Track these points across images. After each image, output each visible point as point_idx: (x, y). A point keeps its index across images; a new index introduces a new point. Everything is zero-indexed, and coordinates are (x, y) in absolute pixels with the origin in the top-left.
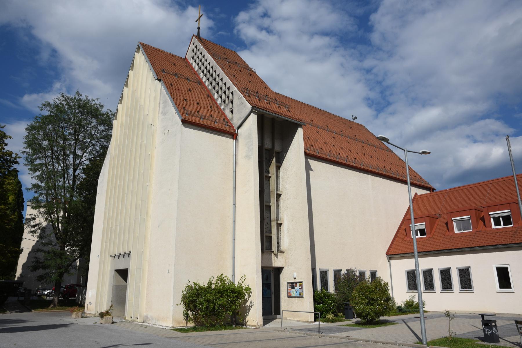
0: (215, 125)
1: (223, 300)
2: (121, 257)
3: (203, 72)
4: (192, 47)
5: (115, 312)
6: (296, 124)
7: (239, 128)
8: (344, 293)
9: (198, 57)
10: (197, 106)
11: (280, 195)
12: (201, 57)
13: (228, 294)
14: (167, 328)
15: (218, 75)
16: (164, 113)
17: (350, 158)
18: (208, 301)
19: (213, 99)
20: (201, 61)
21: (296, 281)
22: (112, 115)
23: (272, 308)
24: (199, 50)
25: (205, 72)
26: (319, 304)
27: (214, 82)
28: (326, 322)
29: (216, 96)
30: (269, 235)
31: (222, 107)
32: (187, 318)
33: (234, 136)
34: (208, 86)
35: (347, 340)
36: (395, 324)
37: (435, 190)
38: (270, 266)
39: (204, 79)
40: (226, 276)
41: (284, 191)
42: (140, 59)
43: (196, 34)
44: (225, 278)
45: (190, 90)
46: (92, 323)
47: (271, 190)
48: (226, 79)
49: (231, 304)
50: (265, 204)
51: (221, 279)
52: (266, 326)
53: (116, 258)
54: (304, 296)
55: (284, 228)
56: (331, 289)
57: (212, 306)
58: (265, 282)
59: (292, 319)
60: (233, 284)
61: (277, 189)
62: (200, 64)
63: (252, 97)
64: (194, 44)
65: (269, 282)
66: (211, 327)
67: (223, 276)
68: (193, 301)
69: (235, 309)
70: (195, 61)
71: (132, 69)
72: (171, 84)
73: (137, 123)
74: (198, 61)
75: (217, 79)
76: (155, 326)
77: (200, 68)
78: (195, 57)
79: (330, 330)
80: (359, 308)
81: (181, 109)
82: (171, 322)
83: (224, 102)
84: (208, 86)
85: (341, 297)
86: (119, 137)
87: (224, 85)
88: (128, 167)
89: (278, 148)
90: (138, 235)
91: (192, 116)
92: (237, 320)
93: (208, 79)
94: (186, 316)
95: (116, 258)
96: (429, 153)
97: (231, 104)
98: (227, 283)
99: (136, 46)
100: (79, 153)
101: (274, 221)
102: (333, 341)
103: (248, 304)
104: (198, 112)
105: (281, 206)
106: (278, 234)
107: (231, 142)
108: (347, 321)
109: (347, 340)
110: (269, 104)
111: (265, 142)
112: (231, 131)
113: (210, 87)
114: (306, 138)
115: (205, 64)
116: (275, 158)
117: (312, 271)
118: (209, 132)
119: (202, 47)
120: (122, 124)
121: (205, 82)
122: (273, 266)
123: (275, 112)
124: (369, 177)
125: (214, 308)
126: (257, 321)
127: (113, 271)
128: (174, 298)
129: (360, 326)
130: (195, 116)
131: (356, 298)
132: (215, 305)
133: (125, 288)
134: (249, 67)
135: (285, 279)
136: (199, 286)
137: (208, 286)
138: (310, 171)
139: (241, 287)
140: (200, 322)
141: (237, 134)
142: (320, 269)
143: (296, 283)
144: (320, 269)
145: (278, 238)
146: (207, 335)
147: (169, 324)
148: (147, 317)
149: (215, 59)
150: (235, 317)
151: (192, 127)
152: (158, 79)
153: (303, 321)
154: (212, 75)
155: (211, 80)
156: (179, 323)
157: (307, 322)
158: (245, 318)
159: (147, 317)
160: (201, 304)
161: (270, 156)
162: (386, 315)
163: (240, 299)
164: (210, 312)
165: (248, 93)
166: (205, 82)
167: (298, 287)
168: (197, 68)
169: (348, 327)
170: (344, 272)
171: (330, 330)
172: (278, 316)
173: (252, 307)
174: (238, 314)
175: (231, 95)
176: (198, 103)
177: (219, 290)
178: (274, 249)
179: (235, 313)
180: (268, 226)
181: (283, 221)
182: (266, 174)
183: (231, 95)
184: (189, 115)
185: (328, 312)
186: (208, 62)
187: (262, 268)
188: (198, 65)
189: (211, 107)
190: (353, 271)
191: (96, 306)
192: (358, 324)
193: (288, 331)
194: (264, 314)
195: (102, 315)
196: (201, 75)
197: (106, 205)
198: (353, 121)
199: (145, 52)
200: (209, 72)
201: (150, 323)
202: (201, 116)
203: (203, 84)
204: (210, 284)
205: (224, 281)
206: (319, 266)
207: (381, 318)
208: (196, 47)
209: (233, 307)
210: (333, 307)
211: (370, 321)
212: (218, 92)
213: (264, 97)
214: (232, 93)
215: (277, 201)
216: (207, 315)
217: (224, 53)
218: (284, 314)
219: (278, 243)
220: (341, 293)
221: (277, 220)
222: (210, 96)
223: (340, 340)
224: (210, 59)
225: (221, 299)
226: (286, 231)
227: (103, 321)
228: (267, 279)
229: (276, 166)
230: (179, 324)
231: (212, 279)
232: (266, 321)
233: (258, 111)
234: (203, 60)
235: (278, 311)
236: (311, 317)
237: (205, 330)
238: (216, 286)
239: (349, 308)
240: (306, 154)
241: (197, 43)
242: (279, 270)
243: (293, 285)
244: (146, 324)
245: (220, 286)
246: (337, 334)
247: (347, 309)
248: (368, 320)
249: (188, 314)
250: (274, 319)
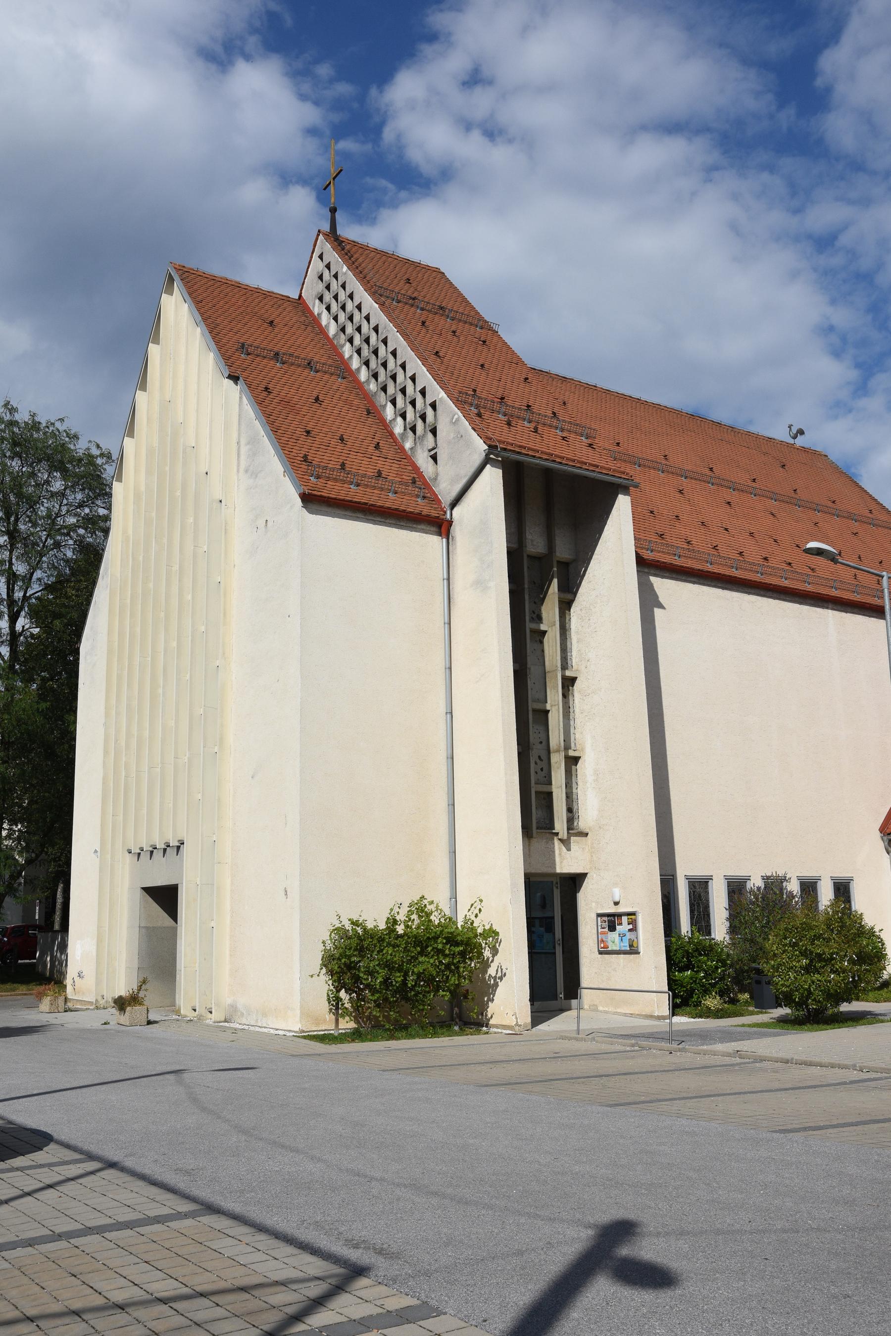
0: (391, 500)
1: (426, 964)
2: (158, 855)
3: (351, 340)
4: (317, 266)
5: (150, 997)
6: (612, 484)
7: (454, 504)
8: (752, 941)
9: (336, 297)
10: (340, 446)
11: (573, 680)
12: (342, 296)
13: (440, 946)
14: (288, 1034)
15: (394, 353)
16: (253, 473)
17: (773, 562)
18: (388, 965)
19: (382, 420)
20: (343, 308)
21: (621, 909)
22: (102, 455)
23: (555, 980)
24: (336, 276)
25: (357, 340)
26: (681, 970)
27: (381, 371)
28: (701, 1017)
29: (389, 412)
30: (544, 788)
31: (408, 445)
32: (337, 1008)
33: (441, 526)
34: (368, 381)
35: (738, 1060)
36: (882, 1021)
38: (550, 871)
39: (355, 363)
40: (432, 903)
41: (582, 668)
42: (176, 310)
43: (326, 227)
44: (429, 907)
45: (317, 399)
46: (97, 1025)
47: (547, 669)
48: (416, 365)
49: (447, 973)
50: (532, 705)
51: (420, 909)
52: (540, 1027)
53: (145, 856)
54: (641, 949)
55: (585, 769)
56: (720, 931)
57: (398, 978)
58: (538, 914)
59: (611, 1009)
60: (451, 921)
61: (565, 666)
62: (342, 317)
63: (486, 415)
64: (321, 257)
65: (548, 914)
66: (399, 1029)
67: (426, 902)
68: (350, 967)
69: (458, 986)
70: (328, 308)
71: (156, 341)
72: (266, 389)
73: (178, 493)
74: (334, 307)
75: (391, 364)
76: (257, 1029)
77: (343, 330)
78: (328, 297)
79: (704, 1036)
80: (783, 981)
81: (299, 463)
82: (298, 1019)
83: (413, 429)
84: (368, 381)
85: (743, 952)
86: (130, 532)
87: (410, 382)
88: (163, 614)
89: (563, 552)
90: (200, 796)
91: (328, 479)
92: (464, 1012)
93: (367, 363)
94: (336, 1004)
95: (145, 856)
97: (430, 436)
98: (435, 919)
99: (163, 278)
100: (20, 568)
101: (558, 751)
102: (700, 1060)
103: (492, 971)
104: (343, 465)
105: (577, 710)
106: (569, 785)
108: (758, 1013)
109: (738, 1060)
110: (536, 430)
111: (529, 536)
112: (434, 513)
113: (373, 387)
114: (642, 519)
115: (357, 318)
116: (555, 581)
117: (663, 882)
118: (375, 523)
119: (345, 268)
120: (137, 496)
121: (358, 370)
122: (558, 871)
123: (551, 457)
124: (831, 617)
125: (404, 983)
126: (515, 1014)
127: (139, 893)
128: (301, 960)
129: (786, 1026)
130: (336, 480)
131: (775, 955)
132: (406, 975)
133: (172, 937)
134: (481, 318)
135: (590, 905)
136: (365, 929)
137: (388, 928)
138: (657, 611)
139: (473, 929)
140: (369, 1018)
141: (450, 523)
142: (687, 878)
143: (620, 915)
144: (687, 878)
145: (570, 797)
146: (389, 1050)
147: (293, 1023)
148: (234, 1008)
149: (382, 305)
150: (459, 1006)
151: (330, 510)
152: (230, 377)
153: (639, 1016)
154: (376, 352)
155: (373, 365)
156: (317, 1021)
157: (651, 1017)
158: (484, 1008)
159: (234, 1008)
160: (371, 973)
161: (542, 575)
162: (858, 999)
163: (471, 959)
164: (396, 992)
165: (477, 407)
166: (358, 370)
167: (624, 927)
168: (332, 330)
169: (755, 1029)
170: (756, 883)
171: (704, 1036)
172: (574, 1002)
173: (501, 978)
174: (466, 997)
175: (430, 412)
176: (342, 439)
177: (415, 937)
178: (560, 825)
179: (458, 996)
180: (543, 764)
181: (583, 750)
182: (533, 626)
183: (430, 412)
184: (318, 477)
185: (706, 992)
186: (365, 312)
187: (526, 875)
188: (336, 319)
189: (377, 446)
190: (784, 879)
191: (98, 982)
192: (783, 1021)
193: (593, 1039)
194: (532, 1000)
195: (121, 1004)
196: (347, 351)
197: (107, 715)
198: (791, 441)
199: (190, 294)
200: (367, 341)
201: (244, 1021)
202: (355, 479)
204: (393, 922)
205: (428, 915)
206: (684, 870)
207: (845, 1007)
208: (328, 266)
209: (453, 980)
210: (722, 979)
211: (815, 1013)
212: (394, 402)
213: (523, 414)
214: (433, 406)
215: (565, 696)
216: (386, 999)
217: (408, 281)
218: (587, 997)
219: (570, 810)
220: (745, 940)
221: (567, 747)
222: (372, 411)
223: (719, 1060)
224: (370, 304)
225: (421, 959)
226: (590, 778)
227: (124, 1019)
228: (544, 906)
229: (561, 602)
230: (317, 1024)
231: (396, 909)
232: (540, 1015)
234: (350, 306)
235: (573, 988)
236: (661, 1004)
237: (384, 1039)
238: (407, 926)
239: (764, 979)
240: (642, 562)
241: (332, 256)
242: (575, 881)
243: (611, 921)
244: (232, 1025)
245: (418, 928)
246: (720, 1047)
247: (758, 982)
248: (808, 1010)
249: (338, 999)
250: (562, 1010)
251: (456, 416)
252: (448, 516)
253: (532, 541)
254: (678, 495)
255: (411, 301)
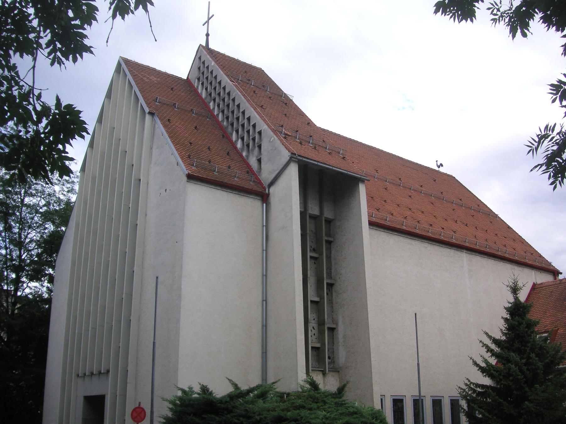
6: (356, 178)
19: (231, 140)
31: (244, 154)
37: (561, 273)
43: (204, 45)
84: (223, 121)
96: (209, 2)
107: (252, 205)
110: (315, 148)
112: (260, 190)
119: (213, 63)
141: (268, 195)
151: (202, 184)
166: (218, 115)
168: (204, 95)
189: (228, 154)
198: (437, 169)
203: (215, 118)
222: (226, 136)
233: (299, 160)
251: (272, 138)
252: (267, 191)
253: (311, 208)
254: (384, 190)
255: (248, 82)
